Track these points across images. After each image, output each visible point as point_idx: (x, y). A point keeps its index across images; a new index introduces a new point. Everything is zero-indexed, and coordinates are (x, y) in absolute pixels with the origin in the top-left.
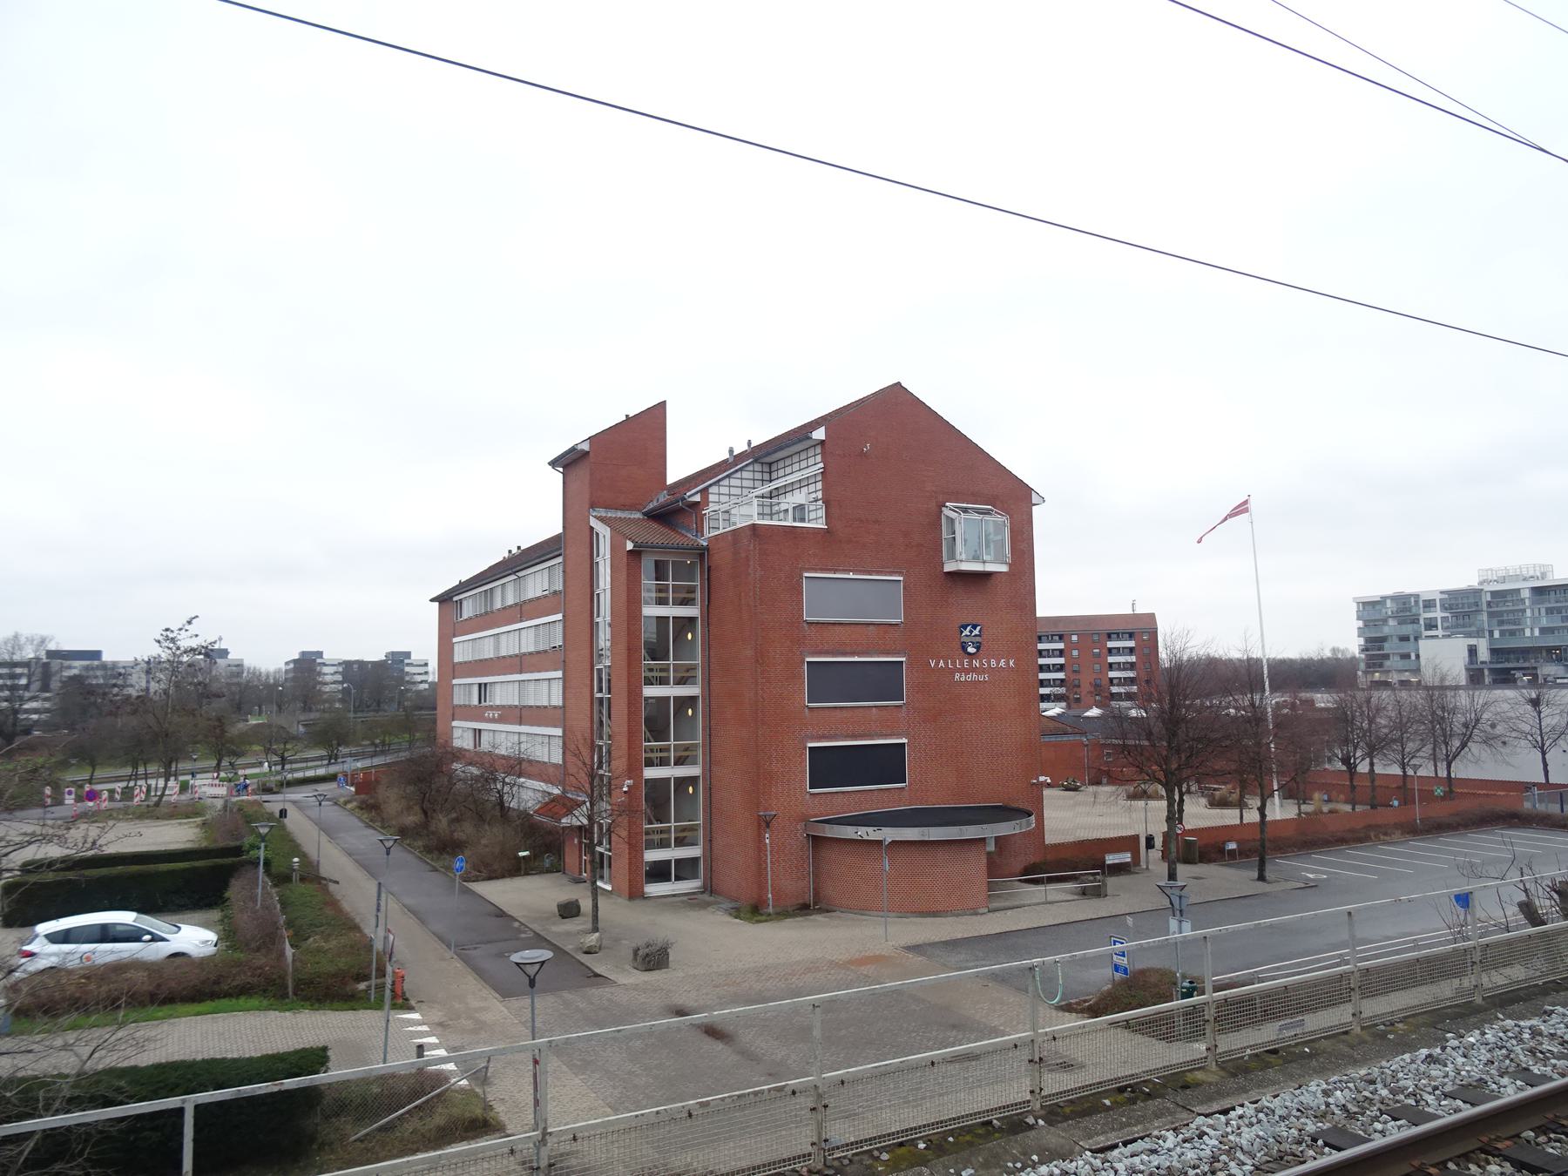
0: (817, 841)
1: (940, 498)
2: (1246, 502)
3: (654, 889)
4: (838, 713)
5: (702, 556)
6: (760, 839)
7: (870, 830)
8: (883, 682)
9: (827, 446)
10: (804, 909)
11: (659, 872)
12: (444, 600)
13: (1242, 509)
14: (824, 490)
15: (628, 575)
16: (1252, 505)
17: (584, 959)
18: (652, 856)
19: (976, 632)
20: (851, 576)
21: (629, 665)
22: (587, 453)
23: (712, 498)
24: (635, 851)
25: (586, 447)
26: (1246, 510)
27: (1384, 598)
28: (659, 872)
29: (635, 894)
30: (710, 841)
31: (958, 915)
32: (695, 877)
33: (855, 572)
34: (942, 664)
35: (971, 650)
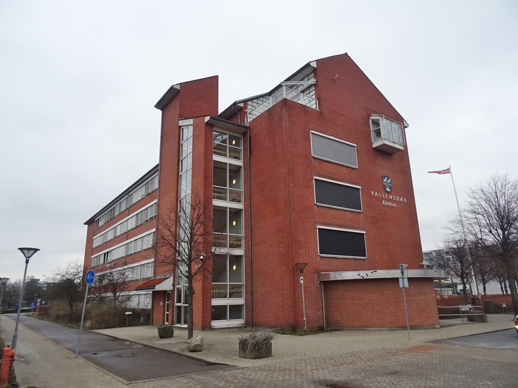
0: (328, 285)
1: (368, 112)
2: (449, 169)
3: (216, 324)
4: (331, 211)
5: (244, 134)
6: (295, 282)
7: (369, 272)
8: (349, 198)
9: (318, 71)
10: (321, 330)
11: (219, 313)
12: (90, 222)
13: (447, 171)
14: (316, 94)
15: (206, 136)
16: (452, 170)
17: (193, 355)
18: (216, 302)
19: (389, 181)
20: (332, 138)
21: (205, 185)
22: (179, 91)
23: (249, 107)
24: (207, 297)
25: (178, 87)
26: (449, 172)
27: (432, 251)
28: (219, 313)
29: (206, 327)
30: (251, 295)
31: (426, 329)
32: (239, 317)
33: (334, 137)
34: (376, 194)
35: (388, 190)
